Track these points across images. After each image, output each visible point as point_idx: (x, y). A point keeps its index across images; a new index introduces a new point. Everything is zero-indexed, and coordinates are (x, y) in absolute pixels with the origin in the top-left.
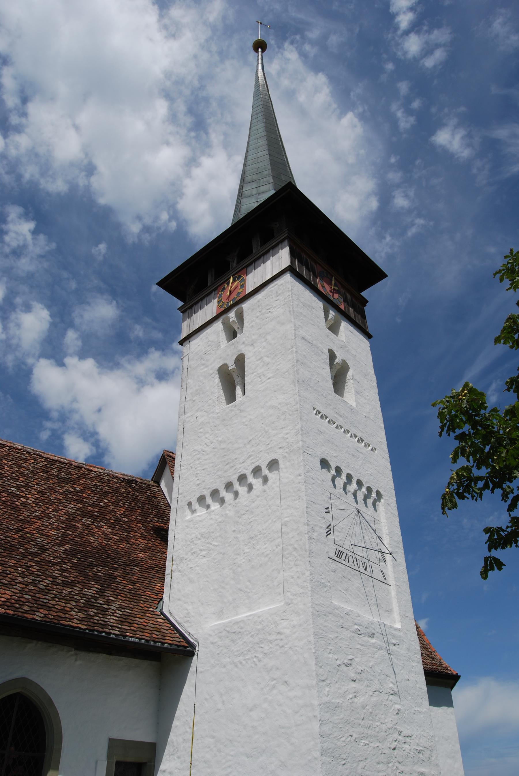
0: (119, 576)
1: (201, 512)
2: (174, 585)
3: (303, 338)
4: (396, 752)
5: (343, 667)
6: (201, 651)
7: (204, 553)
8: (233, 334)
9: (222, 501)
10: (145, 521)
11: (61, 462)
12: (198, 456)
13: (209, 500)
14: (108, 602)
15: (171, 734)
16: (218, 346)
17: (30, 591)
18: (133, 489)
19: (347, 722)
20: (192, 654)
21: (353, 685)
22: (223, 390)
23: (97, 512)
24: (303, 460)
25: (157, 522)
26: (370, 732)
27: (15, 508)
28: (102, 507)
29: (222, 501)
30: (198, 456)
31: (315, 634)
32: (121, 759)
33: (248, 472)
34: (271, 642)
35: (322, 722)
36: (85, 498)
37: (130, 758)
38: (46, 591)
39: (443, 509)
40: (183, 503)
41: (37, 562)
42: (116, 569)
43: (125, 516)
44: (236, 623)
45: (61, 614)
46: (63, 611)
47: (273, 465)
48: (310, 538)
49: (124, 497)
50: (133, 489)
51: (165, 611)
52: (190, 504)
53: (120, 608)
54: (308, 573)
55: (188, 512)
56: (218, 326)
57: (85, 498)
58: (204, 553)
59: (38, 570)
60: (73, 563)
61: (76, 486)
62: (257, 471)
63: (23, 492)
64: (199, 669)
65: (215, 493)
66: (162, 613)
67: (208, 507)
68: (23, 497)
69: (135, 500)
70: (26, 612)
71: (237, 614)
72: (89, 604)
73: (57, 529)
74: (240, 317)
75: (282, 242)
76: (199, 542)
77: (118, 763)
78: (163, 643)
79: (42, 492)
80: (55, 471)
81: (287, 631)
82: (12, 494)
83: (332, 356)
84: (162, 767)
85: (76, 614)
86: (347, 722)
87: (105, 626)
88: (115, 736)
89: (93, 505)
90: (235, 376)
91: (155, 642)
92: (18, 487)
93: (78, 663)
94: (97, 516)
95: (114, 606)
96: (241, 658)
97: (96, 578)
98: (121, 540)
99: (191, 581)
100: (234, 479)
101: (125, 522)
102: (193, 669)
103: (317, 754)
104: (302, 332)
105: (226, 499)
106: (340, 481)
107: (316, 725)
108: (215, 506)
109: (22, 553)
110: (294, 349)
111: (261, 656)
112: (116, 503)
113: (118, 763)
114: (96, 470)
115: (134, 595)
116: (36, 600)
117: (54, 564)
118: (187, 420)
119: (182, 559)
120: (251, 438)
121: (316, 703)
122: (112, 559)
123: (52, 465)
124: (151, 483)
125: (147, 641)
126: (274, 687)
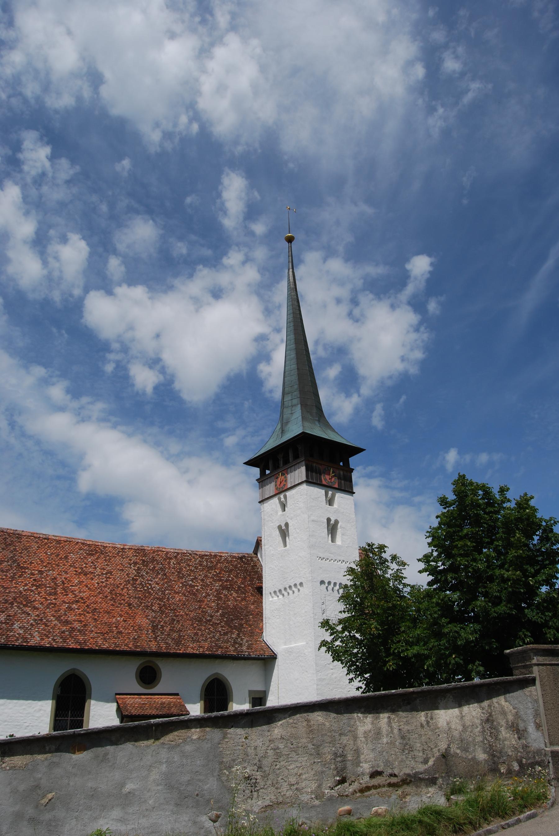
0: (244, 624)
1: (276, 598)
2: (267, 629)
3: (313, 521)
4: (349, 692)
5: (328, 665)
6: (279, 657)
7: (278, 617)
8: (284, 506)
9: (283, 595)
10: (252, 584)
11: (206, 556)
12: (272, 571)
13: (278, 594)
14: (242, 640)
15: (271, 687)
16: (277, 513)
17: (213, 641)
18: (244, 562)
19: (328, 684)
20: (276, 658)
21: (332, 671)
22: (281, 537)
23: (229, 585)
24: (312, 586)
25: (258, 583)
26: (338, 686)
27: (194, 594)
28: (231, 581)
29: (283, 595)
30: (272, 571)
31: (315, 655)
32: (254, 697)
33: (292, 585)
34: (302, 657)
35: (317, 685)
36: (222, 577)
37: (257, 696)
38: (218, 640)
39: (320, 647)
40: (268, 592)
41: (212, 625)
42: (242, 619)
43: (242, 583)
44: (291, 648)
45: (226, 650)
46: (227, 648)
47: (301, 584)
48: (314, 619)
49: (240, 570)
50: (244, 562)
51: (264, 639)
52: (270, 593)
53: (247, 641)
54: (313, 633)
55: (270, 597)
56: (275, 500)
57: (222, 577)
58: (278, 617)
59: (213, 629)
60: (225, 621)
61: (216, 570)
62: (295, 585)
63: (195, 583)
64: (279, 664)
65: (280, 591)
66: (264, 641)
67: (278, 596)
68: (196, 586)
69: (246, 571)
70: (215, 651)
71: (291, 644)
72: (235, 643)
73: (214, 602)
74: (285, 497)
75: (302, 461)
76: (275, 612)
77: (253, 698)
78: (264, 656)
79: (202, 580)
80: (205, 563)
81: (307, 654)
82: (191, 586)
83: (329, 520)
84: (269, 699)
85: (232, 648)
86: (328, 684)
87: (242, 652)
88: (250, 689)
89: (226, 581)
90: (286, 532)
91: (262, 655)
92: (192, 580)
93: (234, 665)
94: (229, 588)
95: (245, 640)
96: (293, 661)
97: (235, 627)
98: (242, 600)
99: (274, 628)
100: (287, 586)
101: (243, 588)
102: (276, 664)
103: (316, 695)
104: (312, 518)
105: (285, 595)
106: (330, 588)
107: (315, 686)
108: (281, 597)
109: (205, 622)
110: (308, 530)
111: (299, 661)
112: (236, 576)
113: (253, 698)
114: (224, 555)
115: (251, 633)
116: (216, 645)
117: (218, 624)
118: (266, 549)
119: (269, 618)
120: (293, 569)
121: (315, 679)
122: (240, 613)
123: (203, 559)
124: (253, 555)
125: (259, 656)
126: (303, 673)
